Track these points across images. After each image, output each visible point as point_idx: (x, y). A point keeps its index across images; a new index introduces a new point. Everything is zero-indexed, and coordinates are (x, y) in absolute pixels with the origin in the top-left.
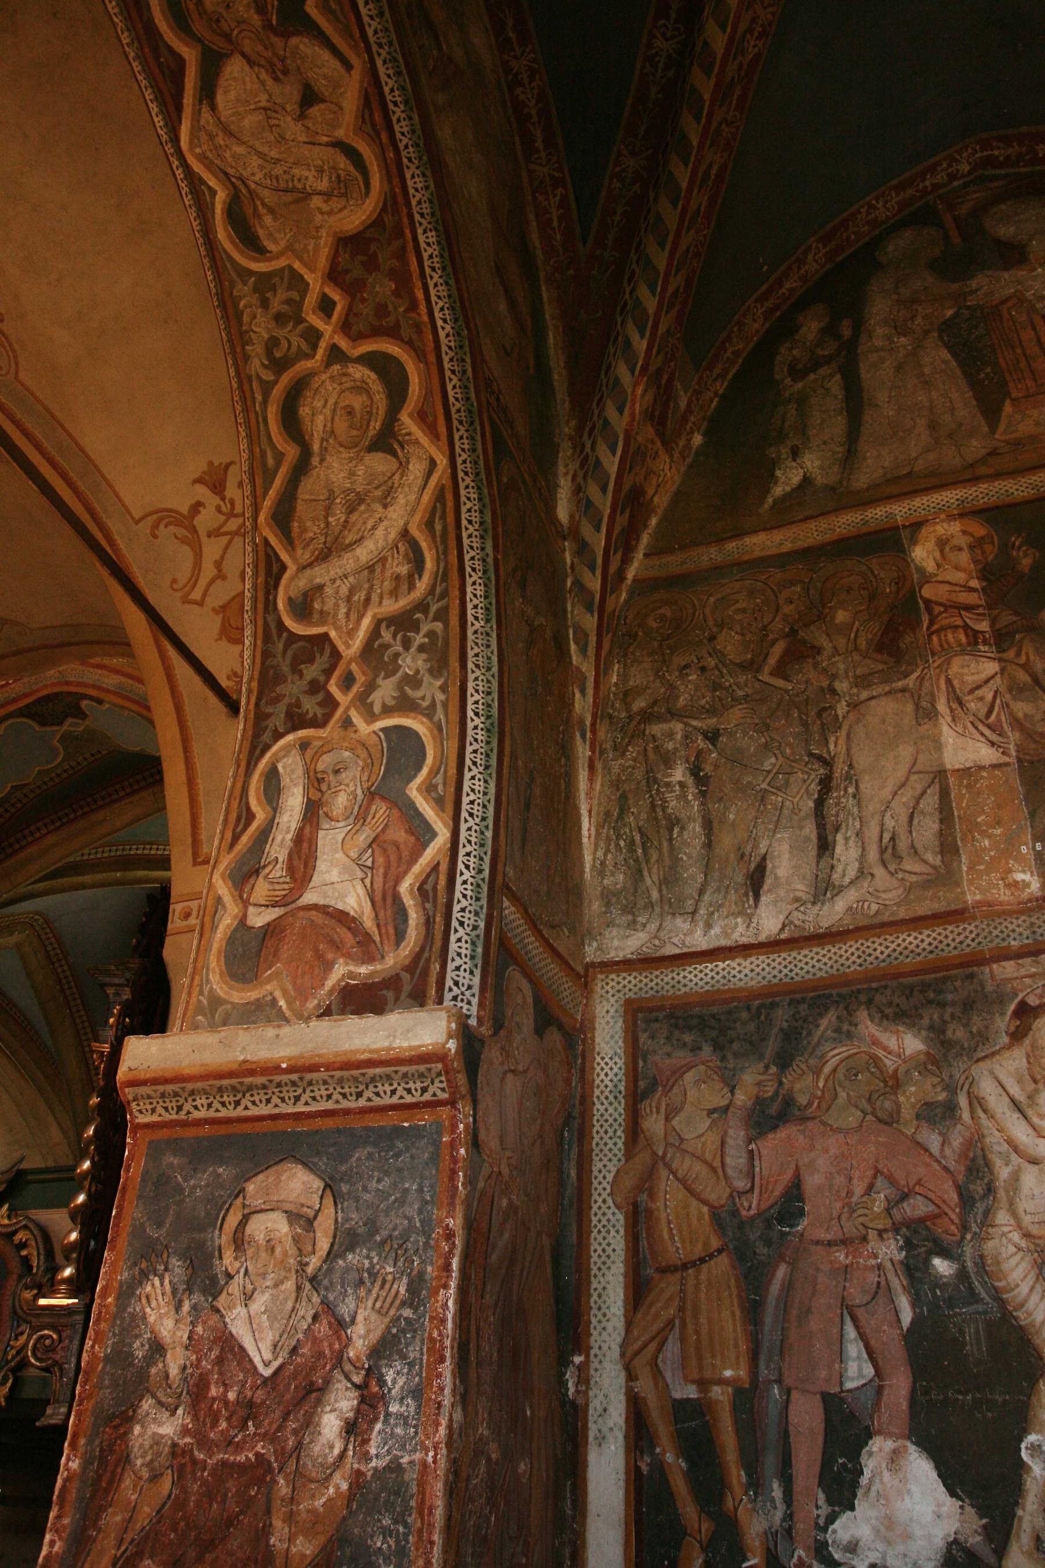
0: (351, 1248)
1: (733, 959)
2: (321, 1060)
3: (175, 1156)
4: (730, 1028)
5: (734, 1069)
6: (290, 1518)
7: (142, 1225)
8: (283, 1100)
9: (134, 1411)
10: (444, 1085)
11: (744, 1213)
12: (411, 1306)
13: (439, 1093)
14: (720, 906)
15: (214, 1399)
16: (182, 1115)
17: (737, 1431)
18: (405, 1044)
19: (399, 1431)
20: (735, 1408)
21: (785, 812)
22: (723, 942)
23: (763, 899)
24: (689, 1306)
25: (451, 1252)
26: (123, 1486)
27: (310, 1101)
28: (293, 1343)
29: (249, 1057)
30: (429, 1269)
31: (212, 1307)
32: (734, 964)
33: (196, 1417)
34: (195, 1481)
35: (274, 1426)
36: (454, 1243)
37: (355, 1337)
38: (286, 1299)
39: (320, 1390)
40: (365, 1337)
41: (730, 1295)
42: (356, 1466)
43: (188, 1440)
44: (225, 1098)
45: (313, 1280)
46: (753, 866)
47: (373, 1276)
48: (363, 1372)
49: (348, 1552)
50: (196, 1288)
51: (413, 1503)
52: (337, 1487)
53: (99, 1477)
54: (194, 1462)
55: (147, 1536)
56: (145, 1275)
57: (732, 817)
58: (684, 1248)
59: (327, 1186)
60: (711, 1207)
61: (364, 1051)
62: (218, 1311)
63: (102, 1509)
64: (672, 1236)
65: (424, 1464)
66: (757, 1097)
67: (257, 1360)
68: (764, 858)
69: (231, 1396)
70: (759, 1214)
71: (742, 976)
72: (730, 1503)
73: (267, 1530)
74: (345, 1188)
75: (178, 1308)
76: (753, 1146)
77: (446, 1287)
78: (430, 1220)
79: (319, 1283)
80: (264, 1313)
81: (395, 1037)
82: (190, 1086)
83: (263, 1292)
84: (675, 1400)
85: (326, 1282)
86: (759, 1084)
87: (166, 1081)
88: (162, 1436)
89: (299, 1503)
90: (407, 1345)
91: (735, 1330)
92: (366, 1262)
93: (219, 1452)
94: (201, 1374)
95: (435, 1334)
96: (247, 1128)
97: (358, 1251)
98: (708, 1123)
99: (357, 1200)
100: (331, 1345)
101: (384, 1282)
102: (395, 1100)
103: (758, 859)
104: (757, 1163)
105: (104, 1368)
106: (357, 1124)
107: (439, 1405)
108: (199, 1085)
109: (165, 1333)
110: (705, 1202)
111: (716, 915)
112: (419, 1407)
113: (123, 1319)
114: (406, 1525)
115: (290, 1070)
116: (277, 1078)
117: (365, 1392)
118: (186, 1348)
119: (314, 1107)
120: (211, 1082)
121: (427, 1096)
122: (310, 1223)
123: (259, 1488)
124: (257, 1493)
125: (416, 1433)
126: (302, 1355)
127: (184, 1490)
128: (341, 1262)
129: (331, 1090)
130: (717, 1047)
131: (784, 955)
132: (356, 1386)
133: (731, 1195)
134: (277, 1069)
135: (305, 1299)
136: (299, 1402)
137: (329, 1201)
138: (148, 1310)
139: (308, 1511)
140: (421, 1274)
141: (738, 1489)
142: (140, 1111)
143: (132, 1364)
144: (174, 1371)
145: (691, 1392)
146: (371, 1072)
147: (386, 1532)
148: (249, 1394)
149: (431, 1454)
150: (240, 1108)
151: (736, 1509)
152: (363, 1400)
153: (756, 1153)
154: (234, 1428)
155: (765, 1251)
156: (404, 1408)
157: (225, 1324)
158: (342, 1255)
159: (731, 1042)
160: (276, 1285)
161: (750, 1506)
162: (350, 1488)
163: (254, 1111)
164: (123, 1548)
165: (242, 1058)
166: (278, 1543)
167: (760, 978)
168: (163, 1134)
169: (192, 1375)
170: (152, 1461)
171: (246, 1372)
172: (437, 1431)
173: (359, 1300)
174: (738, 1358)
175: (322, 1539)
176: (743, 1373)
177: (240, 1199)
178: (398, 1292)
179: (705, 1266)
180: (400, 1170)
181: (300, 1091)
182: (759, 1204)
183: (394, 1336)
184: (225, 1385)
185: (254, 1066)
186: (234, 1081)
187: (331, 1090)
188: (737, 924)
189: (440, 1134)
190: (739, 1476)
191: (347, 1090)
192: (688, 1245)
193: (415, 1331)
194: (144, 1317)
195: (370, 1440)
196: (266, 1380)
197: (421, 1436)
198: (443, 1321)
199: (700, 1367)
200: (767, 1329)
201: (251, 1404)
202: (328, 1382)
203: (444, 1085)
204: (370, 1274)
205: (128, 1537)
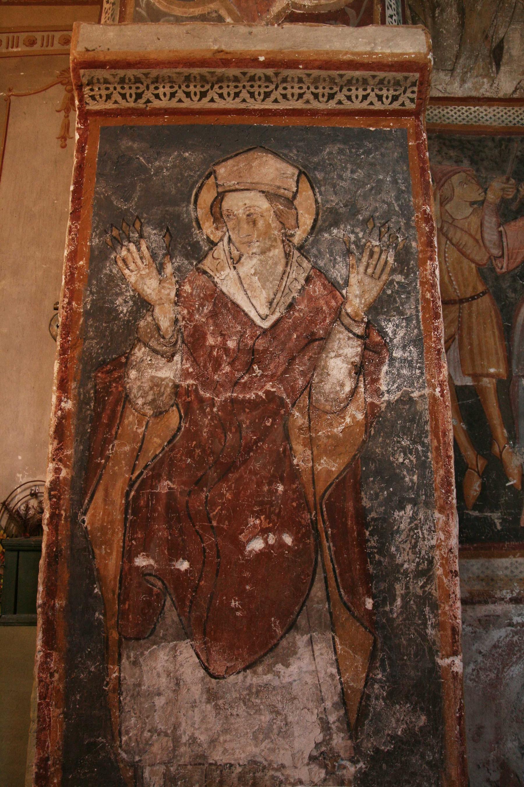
0: (336, 224)
1: (481, 106)
2: (301, 58)
3: (134, 141)
4: (481, 151)
5: (486, 177)
6: (310, 443)
7: (107, 198)
8: (252, 95)
9: (127, 358)
10: (415, 96)
11: (498, 270)
12: (401, 273)
13: (407, 102)
14: (471, 68)
15: (212, 347)
16: (141, 104)
17: (500, 407)
18: (388, 51)
19: (404, 372)
20: (498, 391)
21: (517, 11)
22: (474, 94)
23: (502, 68)
24: (465, 327)
25: (431, 231)
26: (126, 422)
27: (280, 98)
28: (290, 300)
29: (223, 47)
30: (414, 244)
31: (198, 269)
32: (482, 109)
33: (195, 362)
34: (205, 415)
35: (281, 369)
36: (432, 225)
37: (351, 296)
38: (276, 264)
39: (322, 339)
40: (361, 297)
41: (492, 321)
42: (369, 400)
43: (191, 382)
44: (192, 89)
45: (300, 248)
46: (494, 44)
47: (361, 248)
48: (363, 325)
49: (372, 467)
50: (176, 253)
51: (428, 428)
52: (353, 417)
53: (98, 416)
54: (201, 400)
55: (162, 462)
56: (117, 242)
57: (479, 8)
58: (460, 290)
59: (300, 173)
60: (477, 264)
61: (346, 53)
62: (205, 272)
63: (107, 441)
64: (451, 282)
65: (433, 397)
66: (502, 198)
67: (253, 314)
68: (502, 41)
69: (231, 344)
70: (508, 272)
71: (488, 118)
72: (496, 449)
73: (289, 453)
74: (319, 176)
75: (160, 269)
76: (501, 229)
77: (432, 259)
78: (408, 206)
79: (308, 251)
80: (255, 274)
81: (376, 44)
82: (154, 73)
83: (251, 258)
84: (457, 386)
85: (314, 251)
86: (503, 189)
87: (129, 65)
88: (162, 380)
89: (317, 432)
90: (402, 304)
91: (495, 344)
92: (353, 237)
93: (226, 391)
94: (195, 326)
95: (428, 296)
96: (211, 120)
97: (342, 226)
98: (471, 210)
99: (334, 186)
100: (327, 303)
101: (371, 255)
102: (364, 105)
103: (498, 41)
104: (504, 239)
105: (85, 321)
106: (325, 125)
107: (439, 351)
108: (166, 72)
109: (149, 291)
110: (473, 261)
111: (469, 75)
112: (422, 353)
113: (99, 280)
114: (423, 444)
115: (267, 64)
116: (252, 71)
117: (367, 341)
118: (176, 304)
119: (283, 105)
120: (178, 70)
121: (396, 105)
122: (290, 202)
123: (274, 420)
124: (272, 424)
125: (422, 373)
126: (300, 311)
127: (194, 423)
128: (326, 235)
129: (305, 89)
130: (473, 162)
131: (516, 108)
132: (358, 337)
133: (490, 258)
134: (254, 62)
135: (295, 264)
136: (303, 349)
137: (305, 185)
138: (127, 272)
139: (328, 437)
140: (407, 249)
141: (502, 441)
142: (93, 98)
143: (117, 318)
144: (165, 324)
145: (468, 382)
146: (350, 74)
147: (406, 451)
148: (250, 342)
149: (438, 390)
150: (205, 100)
151: (501, 452)
152: (366, 347)
153: (503, 233)
154: (238, 371)
155: (513, 295)
156: (407, 354)
157: (215, 284)
158: (327, 229)
159: (482, 160)
160: (263, 252)
161: (510, 450)
162: (366, 417)
163: (220, 104)
164: (137, 473)
165: (216, 47)
166: (301, 463)
167: (500, 121)
168: (119, 121)
169: (185, 327)
170: (154, 400)
171: (244, 325)
172: (440, 372)
173: (350, 267)
174: (498, 361)
175: (346, 459)
176: (502, 371)
177: (212, 180)
178: (386, 262)
179: (474, 302)
180: (372, 165)
181: (272, 87)
182: (507, 266)
183: (389, 296)
184: (222, 335)
185: (229, 57)
186: (204, 71)
187: (305, 89)
188: (483, 83)
189: (406, 140)
190: (503, 433)
191: (320, 91)
192: (462, 288)
193: (409, 293)
194: (123, 278)
195: (378, 379)
196: (265, 332)
197: (427, 376)
198: (433, 286)
199: (474, 366)
200: (516, 344)
201: (253, 351)
202: (328, 335)
203: (415, 96)
204: (357, 246)
205: (141, 464)
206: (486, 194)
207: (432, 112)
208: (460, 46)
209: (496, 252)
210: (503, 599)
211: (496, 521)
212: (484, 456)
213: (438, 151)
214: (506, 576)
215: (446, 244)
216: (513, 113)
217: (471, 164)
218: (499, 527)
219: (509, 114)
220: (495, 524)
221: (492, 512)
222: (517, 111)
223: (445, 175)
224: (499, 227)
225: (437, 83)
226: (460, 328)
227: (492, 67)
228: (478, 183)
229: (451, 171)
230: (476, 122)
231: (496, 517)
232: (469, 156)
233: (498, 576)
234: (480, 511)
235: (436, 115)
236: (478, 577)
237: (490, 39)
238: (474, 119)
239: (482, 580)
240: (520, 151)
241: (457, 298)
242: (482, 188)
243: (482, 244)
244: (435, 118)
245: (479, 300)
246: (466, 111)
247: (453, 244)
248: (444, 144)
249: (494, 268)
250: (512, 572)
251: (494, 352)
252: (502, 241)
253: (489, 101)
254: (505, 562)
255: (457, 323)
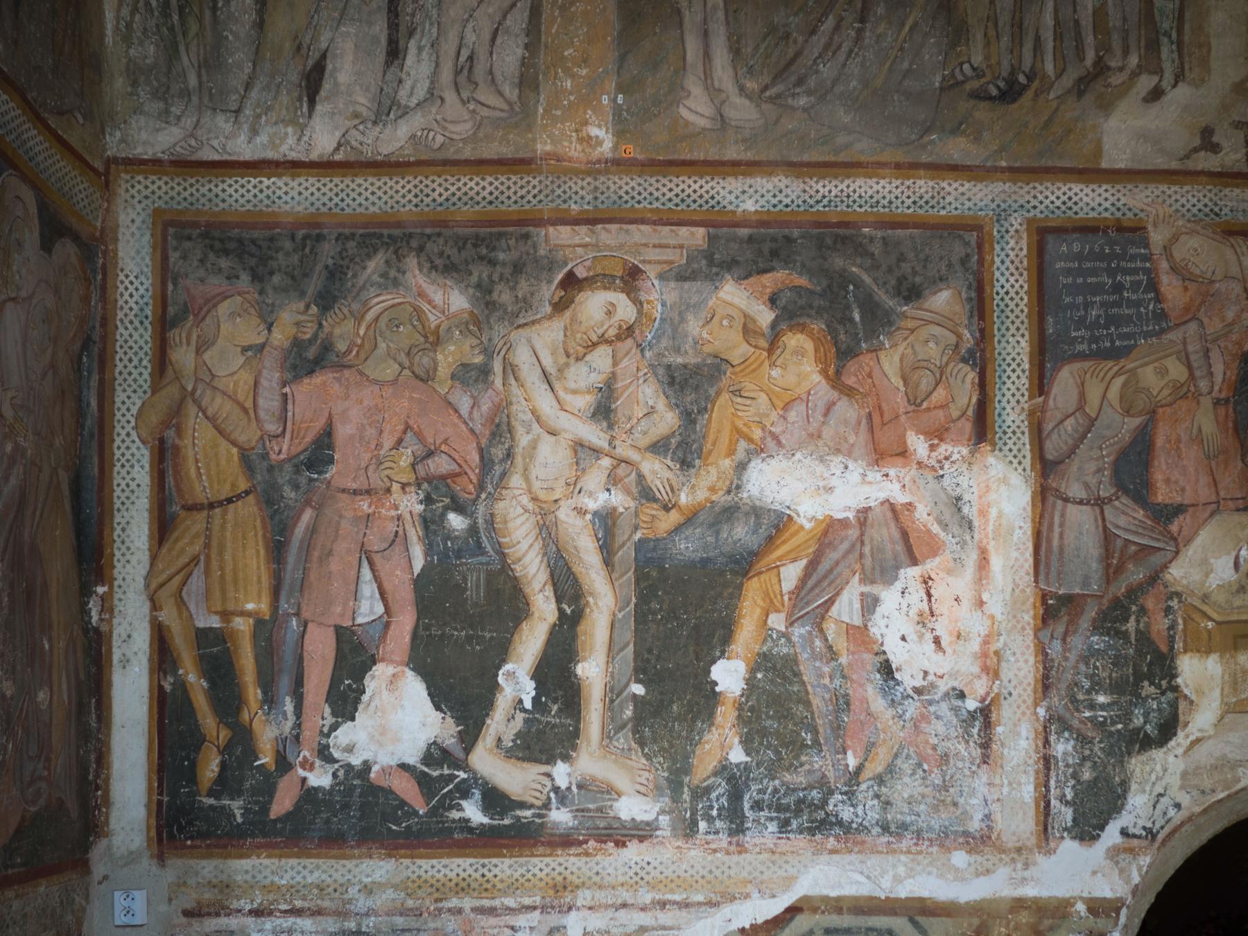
1: (279, 176)
5: (273, 305)
11: (273, 456)
22: (270, 155)
23: (319, 107)
24: (214, 543)
32: (280, 183)
41: (256, 535)
46: (310, 63)
58: (211, 488)
60: (240, 448)
66: (295, 338)
68: (324, 56)
70: (289, 459)
71: (288, 198)
72: (246, 716)
76: (287, 390)
84: (198, 629)
86: (297, 324)
91: (258, 568)
98: (241, 360)
104: (290, 407)
110: (234, 443)
130: (256, 277)
131: (336, 180)
133: (262, 438)
145: (215, 622)
151: (251, 721)
153: (290, 396)
179: (232, 506)
188: (286, 134)
200: (289, 567)
206: (269, 330)
207: (198, 190)
208: (254, 66)
209: (273, 428)
210: (240, 911)
211: (236, 811)
212: (227, 725)
213: (201, 261)
214: (246, 882)
215: (197, 416)
216: (331, 190)
217: (253, 281)
218: (239, 820)
219: (324, 190)
220: (234, 816)
221: (233, 799)
222: (336, 185)
223: (207, 301)
224: (284, 386)
225: (212, 135)
226: (207, 546)
227: (301, 106)
228: (261, 316)
229: (219, 294)
230: (267, 206)
231: (236, 807)
232: (252, 269)
233: (235, 881)
234: (216, 798)
235: (204, 195)
236: (210, 882)
237: (304, 51)
238: (266, 202)
239: (214, 887)
240: (333, 258)
241: (206, 502)
242: (265, 322)
243: (252, 415)
244: (203, 200)
245: (240, 503)
246: (255, 187)
247: (207, 417)
248: (212, 247)
249: (267, 454)
250: (254, 877)
251: (255, 579)
252: (286, 410)
253: (294, 167)
254: (246, 864)
255: (202, 539)
